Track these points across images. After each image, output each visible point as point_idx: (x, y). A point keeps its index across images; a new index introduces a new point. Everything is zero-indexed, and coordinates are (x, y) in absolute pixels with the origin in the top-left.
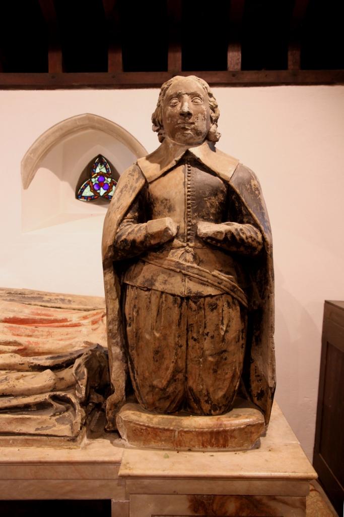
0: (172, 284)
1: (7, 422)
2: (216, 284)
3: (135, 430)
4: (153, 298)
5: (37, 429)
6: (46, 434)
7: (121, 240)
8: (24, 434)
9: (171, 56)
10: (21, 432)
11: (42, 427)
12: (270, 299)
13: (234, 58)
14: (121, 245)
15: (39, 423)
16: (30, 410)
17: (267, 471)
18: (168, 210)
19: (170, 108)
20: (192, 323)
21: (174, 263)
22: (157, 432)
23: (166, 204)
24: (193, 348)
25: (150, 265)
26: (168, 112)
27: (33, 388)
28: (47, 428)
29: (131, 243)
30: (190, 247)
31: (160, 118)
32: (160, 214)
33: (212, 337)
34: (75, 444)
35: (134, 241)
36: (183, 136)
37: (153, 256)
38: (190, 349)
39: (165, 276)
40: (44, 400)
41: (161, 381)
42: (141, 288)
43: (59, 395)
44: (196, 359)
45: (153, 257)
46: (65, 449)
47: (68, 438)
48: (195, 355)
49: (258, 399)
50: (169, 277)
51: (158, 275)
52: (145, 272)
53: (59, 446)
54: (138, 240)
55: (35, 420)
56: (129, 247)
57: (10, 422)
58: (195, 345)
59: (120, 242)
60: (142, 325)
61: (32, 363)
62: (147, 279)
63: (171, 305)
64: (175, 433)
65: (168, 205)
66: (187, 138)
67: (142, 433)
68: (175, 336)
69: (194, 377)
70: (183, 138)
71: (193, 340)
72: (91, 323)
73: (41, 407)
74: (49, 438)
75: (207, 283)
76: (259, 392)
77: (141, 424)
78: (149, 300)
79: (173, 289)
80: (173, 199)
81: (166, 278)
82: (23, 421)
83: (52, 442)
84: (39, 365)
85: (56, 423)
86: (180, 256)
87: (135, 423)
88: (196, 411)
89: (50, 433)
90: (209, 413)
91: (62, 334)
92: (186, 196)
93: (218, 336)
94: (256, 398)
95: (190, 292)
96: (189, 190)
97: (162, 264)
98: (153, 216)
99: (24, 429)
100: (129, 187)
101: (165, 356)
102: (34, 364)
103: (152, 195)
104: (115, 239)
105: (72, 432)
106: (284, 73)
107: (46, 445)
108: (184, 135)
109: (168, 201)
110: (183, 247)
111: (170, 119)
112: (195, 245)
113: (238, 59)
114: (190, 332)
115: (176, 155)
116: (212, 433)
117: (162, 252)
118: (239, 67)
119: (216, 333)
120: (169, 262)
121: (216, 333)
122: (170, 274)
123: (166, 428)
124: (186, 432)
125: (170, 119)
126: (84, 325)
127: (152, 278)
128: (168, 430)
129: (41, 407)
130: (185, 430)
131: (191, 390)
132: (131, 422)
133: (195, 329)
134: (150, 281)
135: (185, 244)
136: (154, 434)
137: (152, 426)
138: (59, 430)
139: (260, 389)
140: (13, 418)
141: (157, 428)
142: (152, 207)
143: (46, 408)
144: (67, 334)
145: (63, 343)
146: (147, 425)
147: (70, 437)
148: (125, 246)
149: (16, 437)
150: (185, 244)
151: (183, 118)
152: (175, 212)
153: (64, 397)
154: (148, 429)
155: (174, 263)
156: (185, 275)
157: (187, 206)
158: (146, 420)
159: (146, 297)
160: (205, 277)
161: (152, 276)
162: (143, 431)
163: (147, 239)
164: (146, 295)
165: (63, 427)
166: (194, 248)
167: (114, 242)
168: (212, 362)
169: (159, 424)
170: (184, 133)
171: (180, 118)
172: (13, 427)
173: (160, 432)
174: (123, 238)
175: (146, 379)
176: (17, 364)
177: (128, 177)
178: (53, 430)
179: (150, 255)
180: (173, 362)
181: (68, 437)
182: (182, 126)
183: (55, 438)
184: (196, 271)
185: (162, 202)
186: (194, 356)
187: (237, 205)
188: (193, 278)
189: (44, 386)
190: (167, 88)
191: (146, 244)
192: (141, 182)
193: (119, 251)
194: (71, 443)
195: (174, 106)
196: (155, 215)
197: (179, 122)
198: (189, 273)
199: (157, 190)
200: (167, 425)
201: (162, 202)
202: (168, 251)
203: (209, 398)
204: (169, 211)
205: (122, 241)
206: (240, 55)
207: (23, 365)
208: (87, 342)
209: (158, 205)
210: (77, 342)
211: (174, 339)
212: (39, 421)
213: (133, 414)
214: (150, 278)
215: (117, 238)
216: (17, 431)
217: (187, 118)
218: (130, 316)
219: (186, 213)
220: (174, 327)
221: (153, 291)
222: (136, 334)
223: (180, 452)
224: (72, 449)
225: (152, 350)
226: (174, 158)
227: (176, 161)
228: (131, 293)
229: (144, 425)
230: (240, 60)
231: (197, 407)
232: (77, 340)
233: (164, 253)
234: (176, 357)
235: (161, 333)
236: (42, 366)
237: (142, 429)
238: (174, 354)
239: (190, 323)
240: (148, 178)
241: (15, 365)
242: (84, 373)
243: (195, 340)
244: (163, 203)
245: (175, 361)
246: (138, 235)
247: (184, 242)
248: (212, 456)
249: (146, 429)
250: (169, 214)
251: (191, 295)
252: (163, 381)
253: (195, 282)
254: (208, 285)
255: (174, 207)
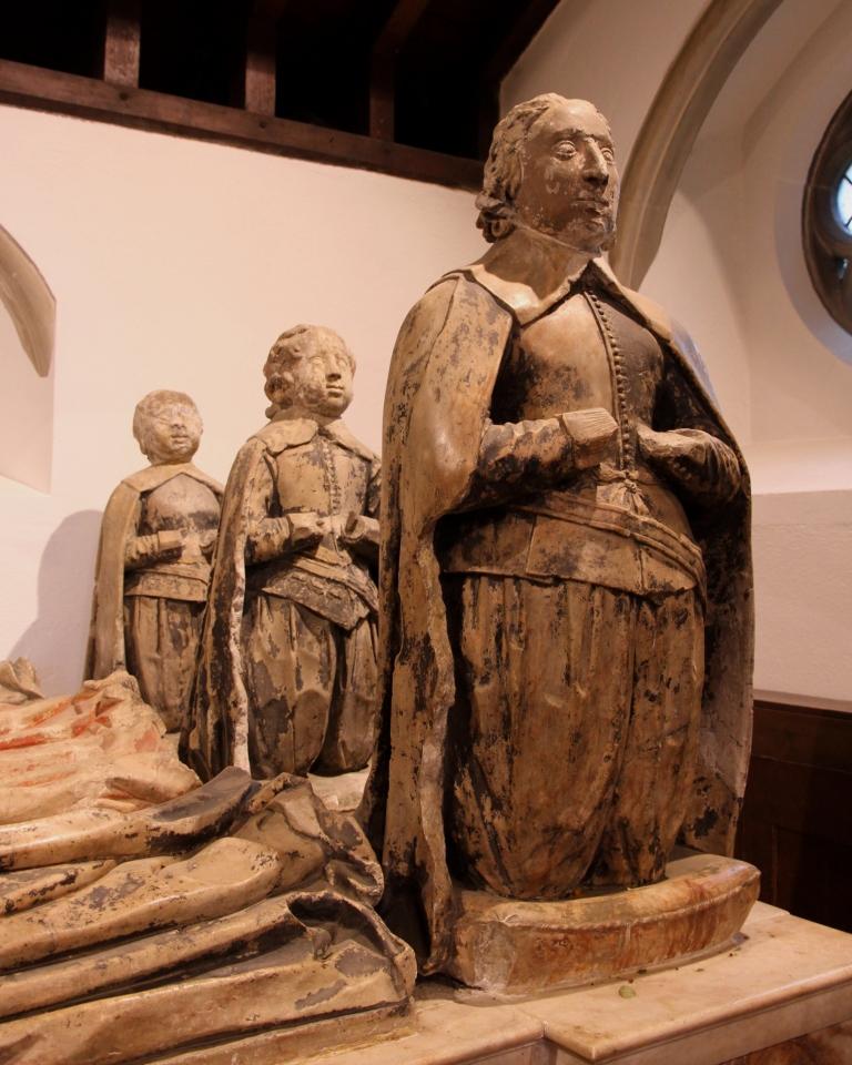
0: (617, 565)
1: (219, 1001)
2: (687, 564)
3: (539, 948)
4: (575, 604)
5: (300, 1003)
6: (329, 1010)
7: (497, 458)
8: (267, 1027)
9: (112, 45)
10: (260, 1020)
11: (309, 994)
12: (750, 599)
13: (259, 84)
14: (494, 472)
15: (301, 985)
16: (240, 957)
17: (836, 967)
18: (574, 393)
19: (556, 160)
20: (645, 657)
21: (615, 516)
22: (588, 941)
23: (569, 379)
24: (645, 719)
25: (554, 521)
26: (549, 173)
27: (231, 891)
28: (325, 994)
29: (527, 467)
30: (633, 480)
31: (516, 178)
32: (552, 403)
33: (676, 690)
34: (407, 1019)
35: (534, 462)
36: (588, 227)
37: (562, 500)
38: (638, 721)
39: (599, 547)
40: (282, 919)
41: (576, 813)
42: (534, 581)
43: (309, 899)
44: (650, 745)
45: (561, 503)
46: (381, 1041)
47: (390, 1009)
48: (647, 736)
49: (697, 835)
50: (608, 549)
51: (582, 546)
52: (536, 545)
53: (365, 1039)
54: (546, 458)
55: (288, 977)
56: (518, 475)
57: (226, 997)
58: (651, 711)
59: (496, 463)
60: (535, 670)
61: (157, 829)
62: (555, 557)
63: (611, 617)
64: (624, 933)
65: (573, 380)
66: (594, 234)
67: (555, 950)
68: (619, 692)
69: (637, 792)
70: (584, 233)
71: (646, 700)
72: (70, 731)
73: (272, 940)
74: (340, 1019)
75: (674, 563)
76: (701, 816)
77: (554, 926)
78: (556, 609)
79: (620, 576)
80: (585, 368)
81: (602, 552)
82: (256, 987)
83: (349, 1032)
84: (172, 832)
85: (342, 976)
86: (618, 497)
87: (539, 930)
88: (621, 880)
89: (339, 1007)
90: (647, 878)
91: (16, 770)
92: (613, 364)
93: (688, 687)
94: (694, 832)
95: (654, 584)
96: (616, 349)
97: (590, 519)
98: (527, 408)
99: (264, 1012)
100: (472, 331)
101: (590, 746)
102: (162, 831)
103: (532, 355)
104: (479, 457)
105: (397, 989)
106: (365, 143)
107: (334, 1042)
108: (591, 226)
109: (572, 373)
110: (620, 479)
111: (558, 184)
112: (641, 475)
113: (269, 91)
114: (641, 681)
115: (568, 267)
116: (691, 917)
117: (578, 490)
118: (270, 108)
119: (684, 678)
120: (608, 513)
121: (684, 678)
122: (608, 541)
123: (608, 924)
124: (645, 926)
125: (558, 184)
126: (51, 739)
127: (567, 554)
128: (611, 929)
129: (272, 940)
130: (645, 920)
131: (624, 825)
132: (528, 928)
133: (652, 672)
134: (563, 559)
135: (622, 473)
136: (582, 946)
137: (577, 927)
138: (362, 992)
139: (705, 808)
140: (232, 984)
141: (588, 931)
142: (528, 386)
143: (283, 944)
144: (30, 768)
145: (45, 790)
146: (566, 926)
147: (396, 1003)
148: (508, 474)
149: (248, 1041)
150: (622, 473)
151: (592, 188)
152: (591, 398)
153: (323, 900)
154: (571, 937)
155: (615, 516)
156: (639, 543)
157: (617, 387)
158: (560, 917)
159: (547, 601)
160: (672, 548)
161: (566, 549)
162: (557, 945)
163: (569, 456)
164: (548, 597)
165: (367, 981)
166: (640, 482)
167: (479, 464)
168: (673, 749)
169: (590, 920)
170: (591, 222)
171: (584, 188)
172: (237, 1011)
173: (596, 938)
174: (503, 453)
175: (537, 813)
176: (120, 836)
177: (462, 307)
178: (346, 995)
179: (551, 499)
180: (608, 757)
181: (388, 1004)
182: (590, 205)
183: (357, 1016)
184: (658, 535)
185: (557, 372)
186: (646, 739)
187: (677, 394)
188: (656, 552)
189: (258, 882)
190: (538, 115)
191: (561, 469)
192: (504, 324)
193: (488, 487)
194: (398, 1020)
195: (565, 158)
196: (536, 405)
197: (582, 194)
198: (649, 540)
199: (540, 342)
200: (607, 918)
201: (557, 373)
202: (590, 487)
203: (657, 838)
204: (577, 396)
205: (502, 460)
206: (274, 81)
207: (134, 839)
208: (117, 779)
209: (545, 380)
210: (86, 785)
211: (616, 699)
212: (301, 978)
213: (520, 908)
214: (562, 552)
215: (486, 452)
216: (249, 1023)
217: (599, 190)
218: (486, 656)
219: (617, 402)
220: (615, 671)
221: (571, 585)
222: (521, 698)
223: (635, 981)
224: (398, 1038)
225: (566, 734)
226: (566, 275)
227: (570, 282)
228: (484, 602)
229: (560, 930)
230: (273, 94)
231: (626, 868)
232: (84, 777)
233: (583, 492)
234: (616, 745)
235: (589, 689)
236: (178, 835)
237: (555, 941)
238: (610, 738)
239: (642, 656)
240: (521, 314)
241: (115, 839)
242: (351, 827)
243: (652, 698)
244: (562, 376)
245: (613, 755)
246: (546, 446)
247: (618, 468)
248: (700, 970)
249: (566, 939)
250: (578, 403)
251: (657, 590)
252: (581, 811)
253: (658, 559)
254: (676, 568)
255: (588, 388)
